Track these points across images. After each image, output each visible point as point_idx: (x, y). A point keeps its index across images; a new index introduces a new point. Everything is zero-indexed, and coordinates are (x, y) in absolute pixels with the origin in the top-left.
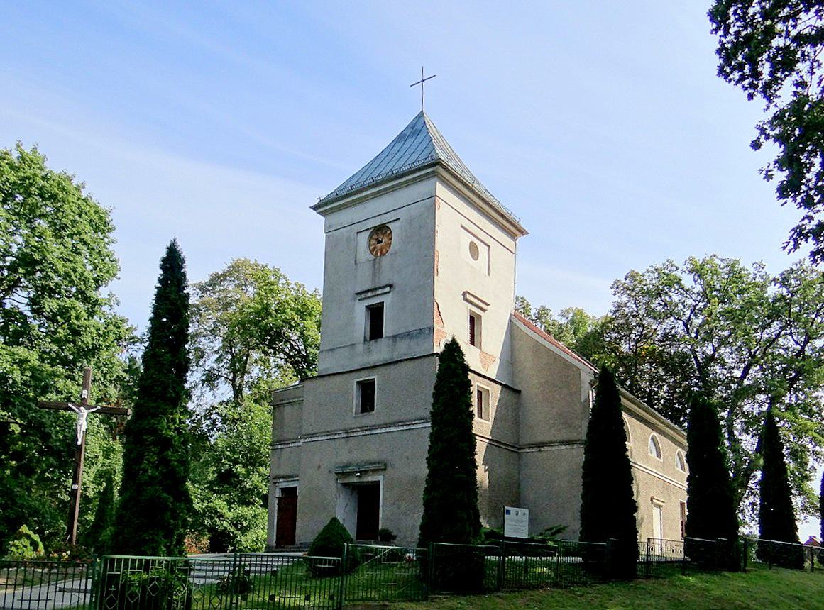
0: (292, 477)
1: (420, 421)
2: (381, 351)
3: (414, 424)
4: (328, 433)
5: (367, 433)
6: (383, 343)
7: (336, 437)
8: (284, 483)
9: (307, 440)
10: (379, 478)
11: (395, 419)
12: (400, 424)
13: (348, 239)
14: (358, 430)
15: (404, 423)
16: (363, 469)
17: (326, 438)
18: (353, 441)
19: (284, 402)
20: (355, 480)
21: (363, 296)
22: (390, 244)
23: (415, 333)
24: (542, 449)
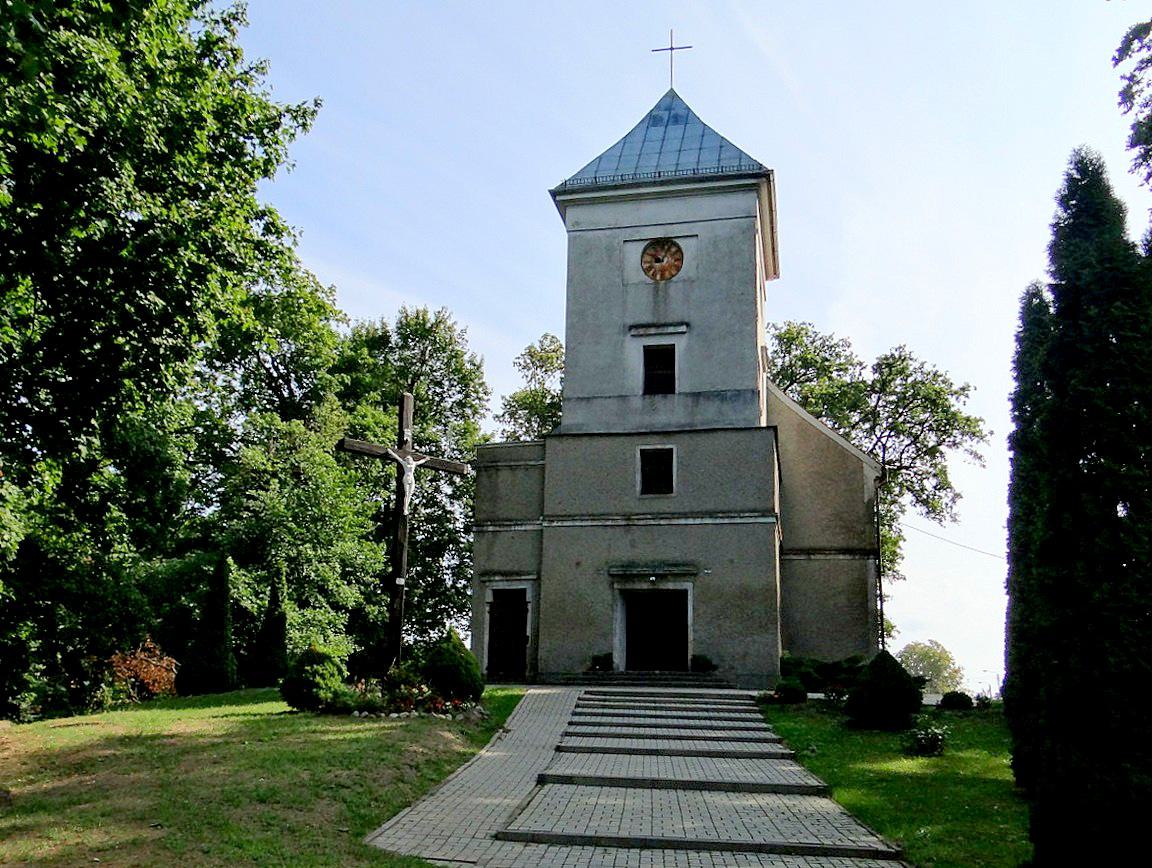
0: (518, 574)
1: (752, 514)
2: (670, 412)
3: (741, 517)
4: (593, 517)
5: (662, 522)
6: (675, 401)
7: (609, 523)
8: (501, 583)
9: (555, 524)
10: (688, 586)
11: (710, 506)
12: (720, 515)
13: (610, 249)
14: (649, 516)
15: (726, 513)
16: (661, 572)
17: (589, 523)
18: (637, 533)
19: (499, 464)
20: (645, 586)
21: (641, 331)
22: (678, 269)
23: (729, 394)
24: (812, 557)
